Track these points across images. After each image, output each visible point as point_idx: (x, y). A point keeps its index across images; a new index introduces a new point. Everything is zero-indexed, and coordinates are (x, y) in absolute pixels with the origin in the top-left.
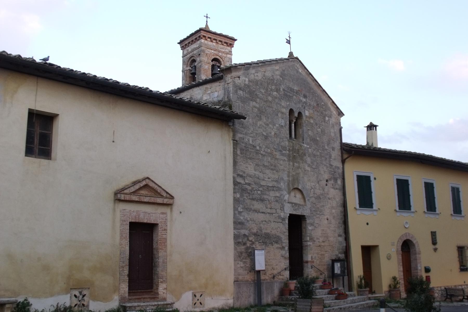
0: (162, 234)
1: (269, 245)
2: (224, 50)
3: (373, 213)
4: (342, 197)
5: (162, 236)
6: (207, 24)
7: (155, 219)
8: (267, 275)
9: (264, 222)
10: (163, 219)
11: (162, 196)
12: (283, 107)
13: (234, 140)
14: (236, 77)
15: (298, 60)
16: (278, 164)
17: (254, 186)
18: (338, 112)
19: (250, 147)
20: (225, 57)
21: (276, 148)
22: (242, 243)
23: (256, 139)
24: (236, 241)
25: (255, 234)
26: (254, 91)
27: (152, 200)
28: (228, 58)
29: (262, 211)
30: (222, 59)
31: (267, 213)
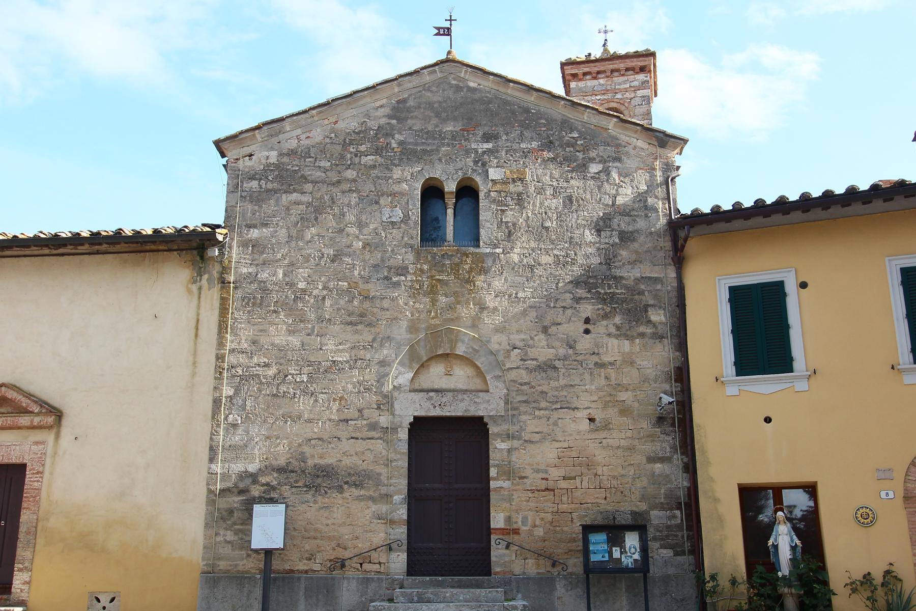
0: (30, 481)
3: (791, 385)
5: (31, 485)
7: (20, 455)
8: (317, 561)
10: (37, 454)
11: (32, 412)
15: (455, 64)
18: (656, 137)
20: (631, 100)
22: (236, 490)
27: (9, 422)
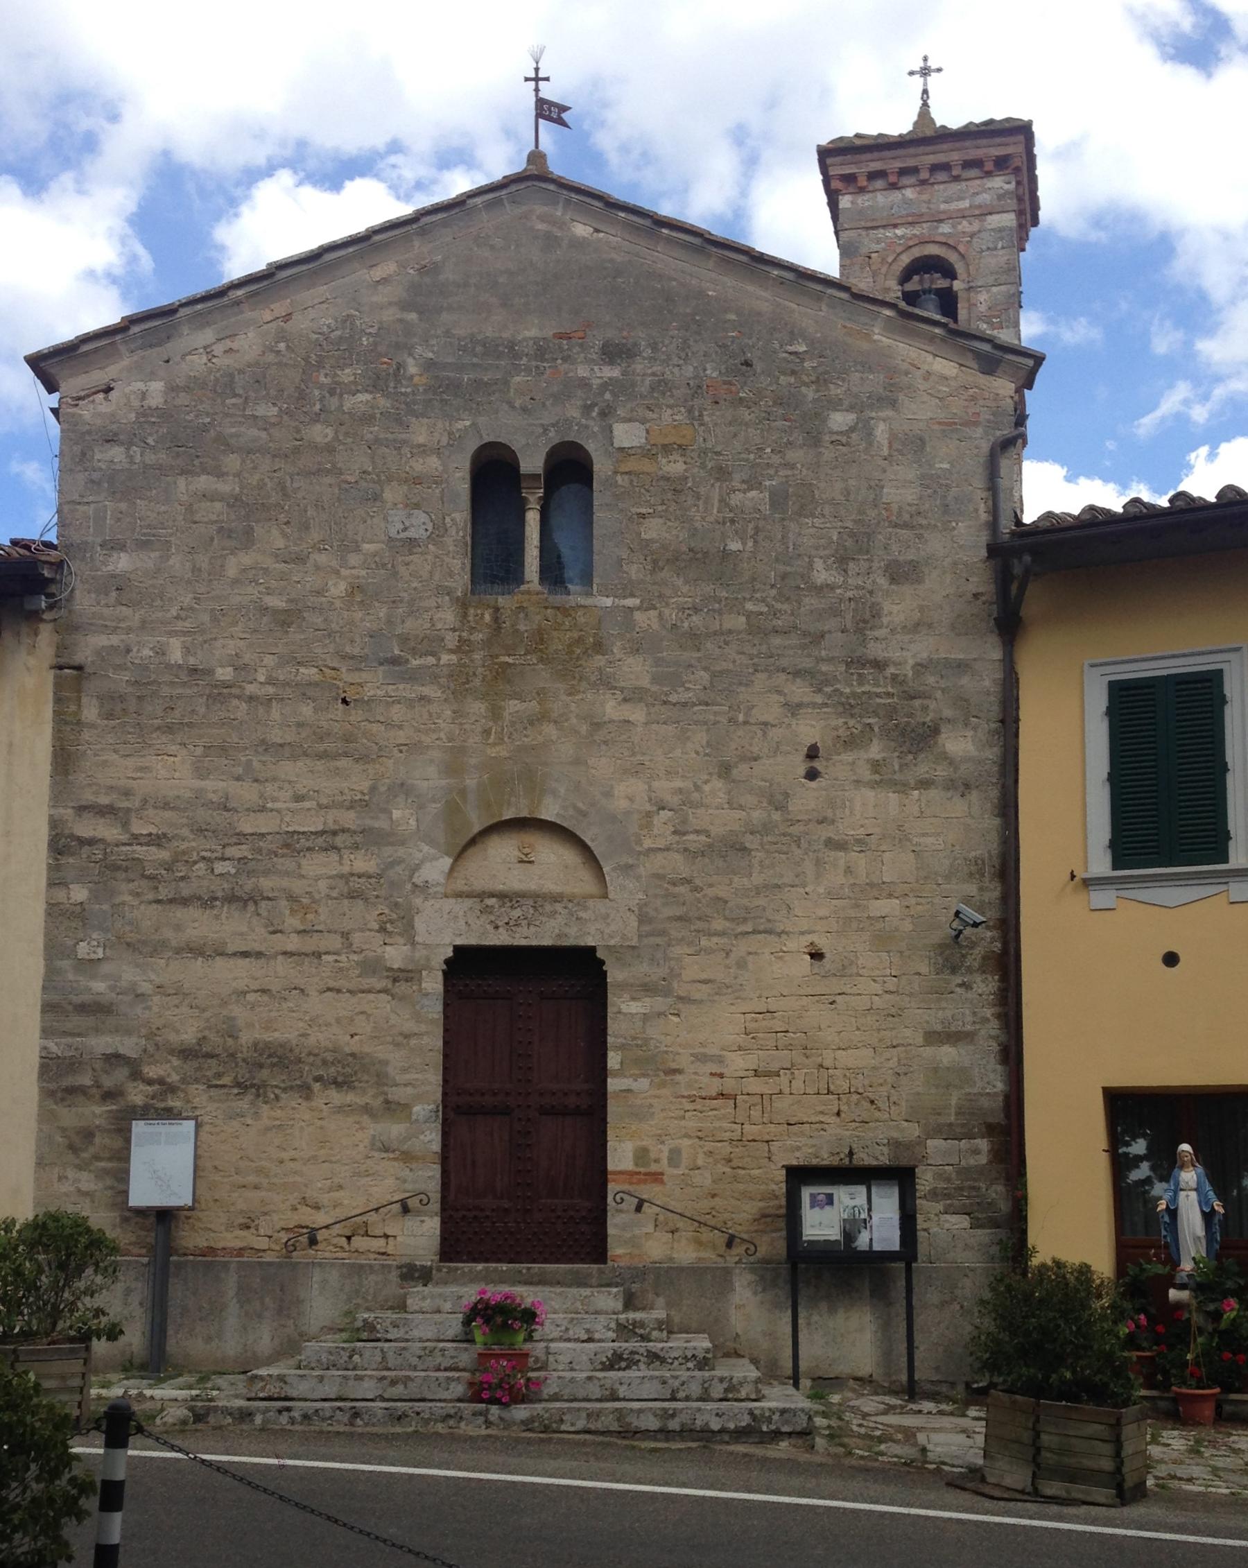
1: (283, 1096)
2: (965, 204)
4: (993, 824)
6: (925, 105)
8: (262, 1232)
9: (251, 997)
12: (423, 450)
13: (61, 668)
14: (83, 394)
15: (544, 185)
16: (375, 728)
17: (194, 844)
19: (167, 678)
21: (356, 651)
23: (215, 639)
24: (53, 1086)
25: (186, 1053)
26: (205, 428)
28: (992, 230)
29: (244, 949)
30: (955, 248)
31: (275, 956)
